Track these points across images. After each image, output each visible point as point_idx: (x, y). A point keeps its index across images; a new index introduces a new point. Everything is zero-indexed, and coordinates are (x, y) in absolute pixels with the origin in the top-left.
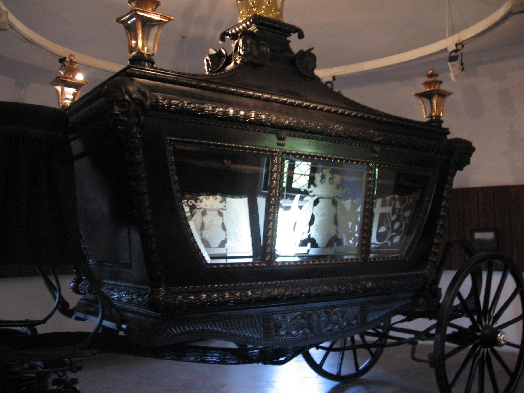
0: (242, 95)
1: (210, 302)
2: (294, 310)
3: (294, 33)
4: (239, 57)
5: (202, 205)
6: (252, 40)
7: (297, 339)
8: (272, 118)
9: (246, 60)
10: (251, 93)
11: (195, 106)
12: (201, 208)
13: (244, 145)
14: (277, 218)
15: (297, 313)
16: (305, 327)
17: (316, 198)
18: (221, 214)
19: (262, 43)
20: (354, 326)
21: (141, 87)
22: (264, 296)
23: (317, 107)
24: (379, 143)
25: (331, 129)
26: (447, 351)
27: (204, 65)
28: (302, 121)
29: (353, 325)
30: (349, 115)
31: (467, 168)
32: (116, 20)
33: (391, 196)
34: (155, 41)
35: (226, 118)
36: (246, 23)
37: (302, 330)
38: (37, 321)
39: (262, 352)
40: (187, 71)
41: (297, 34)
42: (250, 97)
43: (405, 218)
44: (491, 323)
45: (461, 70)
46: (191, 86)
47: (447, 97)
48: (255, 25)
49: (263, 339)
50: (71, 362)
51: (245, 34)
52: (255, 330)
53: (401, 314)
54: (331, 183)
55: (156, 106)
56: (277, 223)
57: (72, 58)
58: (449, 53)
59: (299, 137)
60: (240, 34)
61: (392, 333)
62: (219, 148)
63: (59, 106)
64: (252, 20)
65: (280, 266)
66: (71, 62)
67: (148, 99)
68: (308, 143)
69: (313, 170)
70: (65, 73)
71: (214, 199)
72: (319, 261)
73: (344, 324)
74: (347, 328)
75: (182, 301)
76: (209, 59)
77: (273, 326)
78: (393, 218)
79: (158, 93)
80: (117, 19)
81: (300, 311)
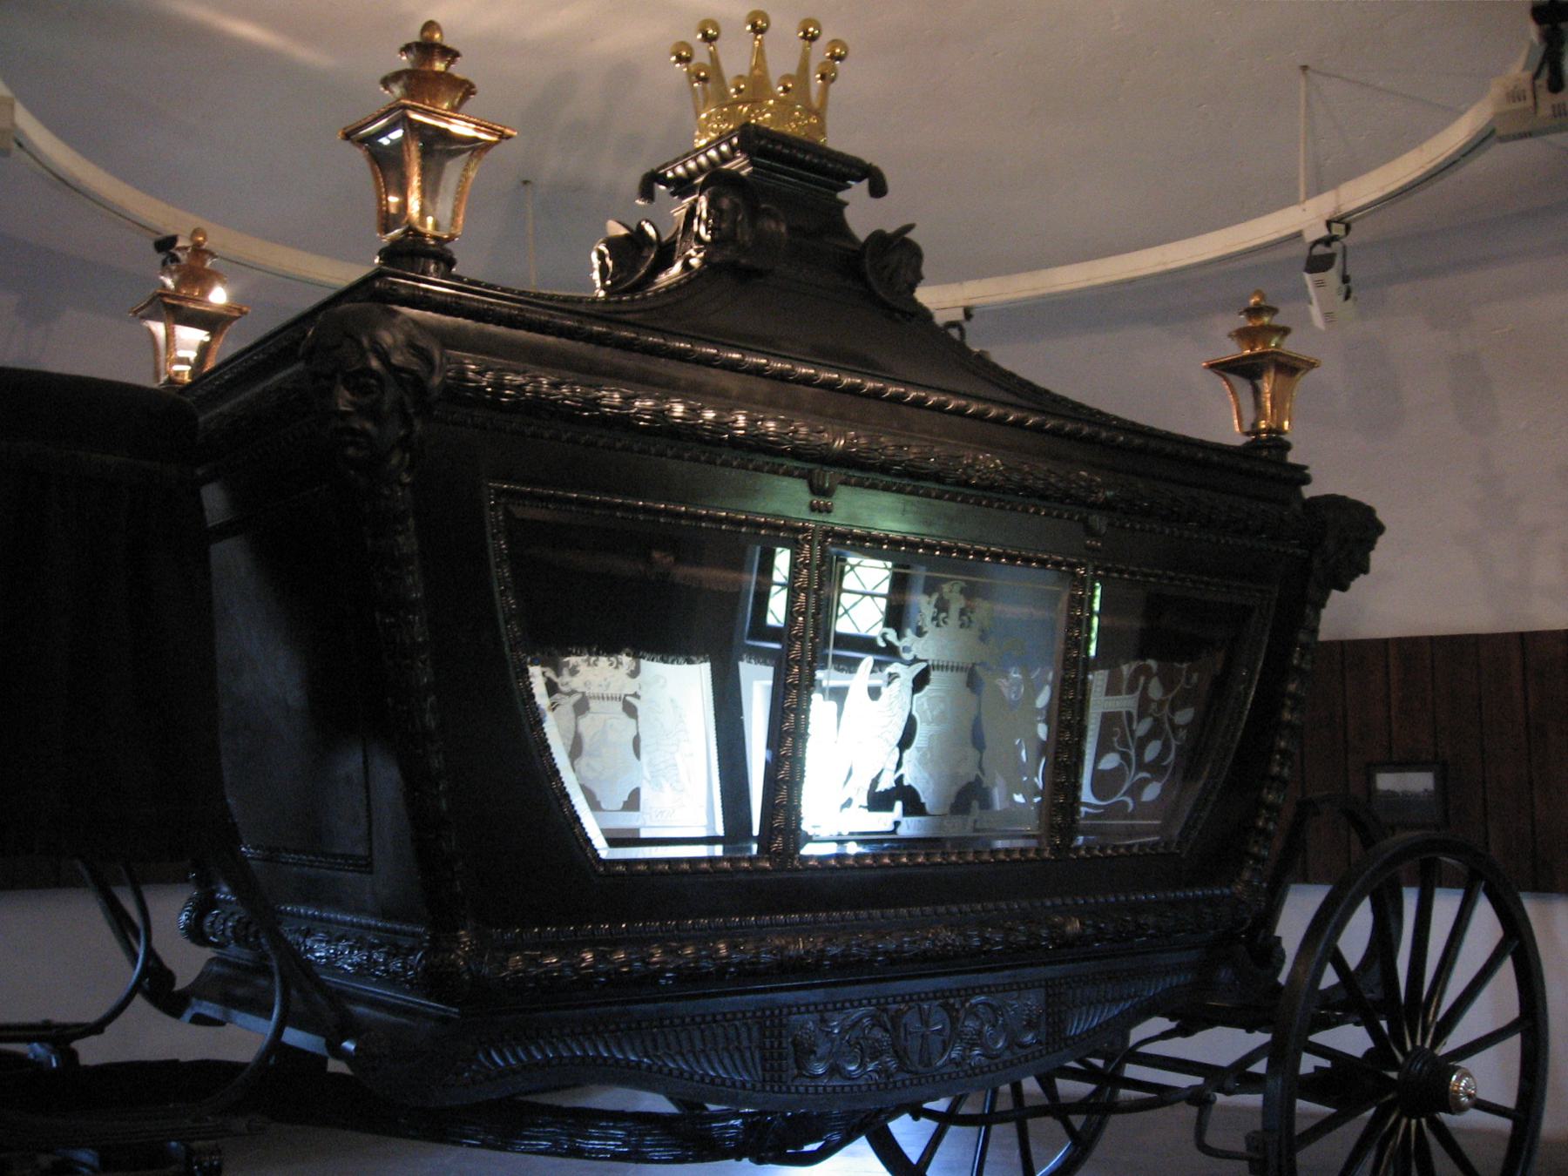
0: (708, 362)
1: (607, 974)
2: (851, 1002)
3: (859, 180)
4: (696, 247)
5: (576, 683)
6: (737, 200)
7: (859, 1086)
8: (795, 432)
9: (717, 259)
10: (736, 356)
11: (573, 391)
12: (573, 692)
13: (713, 508)
14: (807, 724)
15: (861, 1011)
16: (882, 1053)
17: (921, 666)
18: (630, 710)
19: (765, 209)
20: (1028, 1051)
21: (415, 332)
22: (765, 957)
23: (925, 399)
24: (1107, 506)
25: (968, 465)
26: (1301, 1126)
27: (592, 270)
28: (882, 439)
29: (1023, 1046)
30: (1019, 424)
31: (1359, 584)
32: (343, 133)
33: (1134, 665)
34: (458, 200)
35: (663, 428)
36: (717, 148)
37: (872, 1060)
38: (78, 1025)
39: (751, 1124)
40: (533, 286)
41: (865, 183)
42: (733, 367)
43: (1175, 728)
44: (1427, 1045)
45: (1341, 298)
46: (561, 332)
47: (1303, 375)
48: (744, 156)
49: (759, 1086)
50: (190, 1153)
51: (717, 180)
52: (738, 1063)
53: (1163, 1015)
54: (966, 625)
55: (459, 392)
56: (805, 741)
57: (201, 239)
58: (1308, 246)
59: (873, 486)
60: (700, 180)
61: (1132, 1071)
62: (641, 517)
63: (158, 381)
64: (735, 141)
65: (813, 868)
66: (198, 251)
67: (437, 370)
68: (900, 506)
69: (900, 583)
70: (177, 284)
71: (611, 665)
72: (927, 855)
73: (999, 1045)
74: (1007, 1056)
75: (524, 972)
76: (606, 251)
77: (791, 1049)
78: (1142, 728)
79: (468, 351)
80: (346, 131)
81: (870, 1004)
